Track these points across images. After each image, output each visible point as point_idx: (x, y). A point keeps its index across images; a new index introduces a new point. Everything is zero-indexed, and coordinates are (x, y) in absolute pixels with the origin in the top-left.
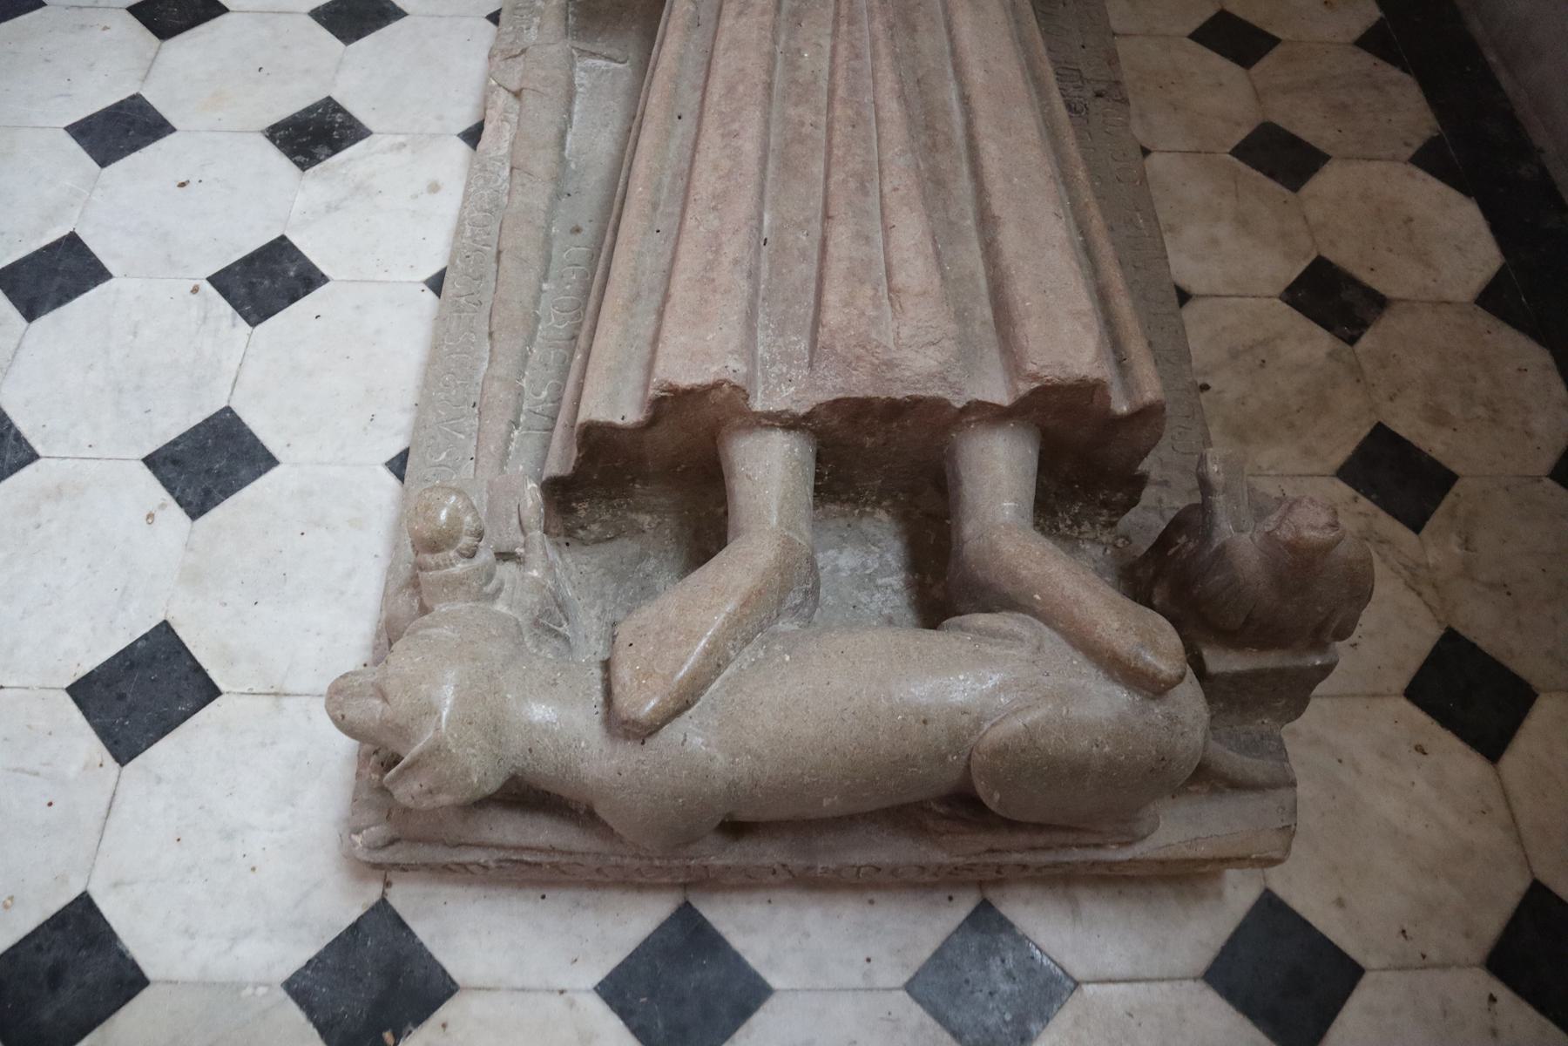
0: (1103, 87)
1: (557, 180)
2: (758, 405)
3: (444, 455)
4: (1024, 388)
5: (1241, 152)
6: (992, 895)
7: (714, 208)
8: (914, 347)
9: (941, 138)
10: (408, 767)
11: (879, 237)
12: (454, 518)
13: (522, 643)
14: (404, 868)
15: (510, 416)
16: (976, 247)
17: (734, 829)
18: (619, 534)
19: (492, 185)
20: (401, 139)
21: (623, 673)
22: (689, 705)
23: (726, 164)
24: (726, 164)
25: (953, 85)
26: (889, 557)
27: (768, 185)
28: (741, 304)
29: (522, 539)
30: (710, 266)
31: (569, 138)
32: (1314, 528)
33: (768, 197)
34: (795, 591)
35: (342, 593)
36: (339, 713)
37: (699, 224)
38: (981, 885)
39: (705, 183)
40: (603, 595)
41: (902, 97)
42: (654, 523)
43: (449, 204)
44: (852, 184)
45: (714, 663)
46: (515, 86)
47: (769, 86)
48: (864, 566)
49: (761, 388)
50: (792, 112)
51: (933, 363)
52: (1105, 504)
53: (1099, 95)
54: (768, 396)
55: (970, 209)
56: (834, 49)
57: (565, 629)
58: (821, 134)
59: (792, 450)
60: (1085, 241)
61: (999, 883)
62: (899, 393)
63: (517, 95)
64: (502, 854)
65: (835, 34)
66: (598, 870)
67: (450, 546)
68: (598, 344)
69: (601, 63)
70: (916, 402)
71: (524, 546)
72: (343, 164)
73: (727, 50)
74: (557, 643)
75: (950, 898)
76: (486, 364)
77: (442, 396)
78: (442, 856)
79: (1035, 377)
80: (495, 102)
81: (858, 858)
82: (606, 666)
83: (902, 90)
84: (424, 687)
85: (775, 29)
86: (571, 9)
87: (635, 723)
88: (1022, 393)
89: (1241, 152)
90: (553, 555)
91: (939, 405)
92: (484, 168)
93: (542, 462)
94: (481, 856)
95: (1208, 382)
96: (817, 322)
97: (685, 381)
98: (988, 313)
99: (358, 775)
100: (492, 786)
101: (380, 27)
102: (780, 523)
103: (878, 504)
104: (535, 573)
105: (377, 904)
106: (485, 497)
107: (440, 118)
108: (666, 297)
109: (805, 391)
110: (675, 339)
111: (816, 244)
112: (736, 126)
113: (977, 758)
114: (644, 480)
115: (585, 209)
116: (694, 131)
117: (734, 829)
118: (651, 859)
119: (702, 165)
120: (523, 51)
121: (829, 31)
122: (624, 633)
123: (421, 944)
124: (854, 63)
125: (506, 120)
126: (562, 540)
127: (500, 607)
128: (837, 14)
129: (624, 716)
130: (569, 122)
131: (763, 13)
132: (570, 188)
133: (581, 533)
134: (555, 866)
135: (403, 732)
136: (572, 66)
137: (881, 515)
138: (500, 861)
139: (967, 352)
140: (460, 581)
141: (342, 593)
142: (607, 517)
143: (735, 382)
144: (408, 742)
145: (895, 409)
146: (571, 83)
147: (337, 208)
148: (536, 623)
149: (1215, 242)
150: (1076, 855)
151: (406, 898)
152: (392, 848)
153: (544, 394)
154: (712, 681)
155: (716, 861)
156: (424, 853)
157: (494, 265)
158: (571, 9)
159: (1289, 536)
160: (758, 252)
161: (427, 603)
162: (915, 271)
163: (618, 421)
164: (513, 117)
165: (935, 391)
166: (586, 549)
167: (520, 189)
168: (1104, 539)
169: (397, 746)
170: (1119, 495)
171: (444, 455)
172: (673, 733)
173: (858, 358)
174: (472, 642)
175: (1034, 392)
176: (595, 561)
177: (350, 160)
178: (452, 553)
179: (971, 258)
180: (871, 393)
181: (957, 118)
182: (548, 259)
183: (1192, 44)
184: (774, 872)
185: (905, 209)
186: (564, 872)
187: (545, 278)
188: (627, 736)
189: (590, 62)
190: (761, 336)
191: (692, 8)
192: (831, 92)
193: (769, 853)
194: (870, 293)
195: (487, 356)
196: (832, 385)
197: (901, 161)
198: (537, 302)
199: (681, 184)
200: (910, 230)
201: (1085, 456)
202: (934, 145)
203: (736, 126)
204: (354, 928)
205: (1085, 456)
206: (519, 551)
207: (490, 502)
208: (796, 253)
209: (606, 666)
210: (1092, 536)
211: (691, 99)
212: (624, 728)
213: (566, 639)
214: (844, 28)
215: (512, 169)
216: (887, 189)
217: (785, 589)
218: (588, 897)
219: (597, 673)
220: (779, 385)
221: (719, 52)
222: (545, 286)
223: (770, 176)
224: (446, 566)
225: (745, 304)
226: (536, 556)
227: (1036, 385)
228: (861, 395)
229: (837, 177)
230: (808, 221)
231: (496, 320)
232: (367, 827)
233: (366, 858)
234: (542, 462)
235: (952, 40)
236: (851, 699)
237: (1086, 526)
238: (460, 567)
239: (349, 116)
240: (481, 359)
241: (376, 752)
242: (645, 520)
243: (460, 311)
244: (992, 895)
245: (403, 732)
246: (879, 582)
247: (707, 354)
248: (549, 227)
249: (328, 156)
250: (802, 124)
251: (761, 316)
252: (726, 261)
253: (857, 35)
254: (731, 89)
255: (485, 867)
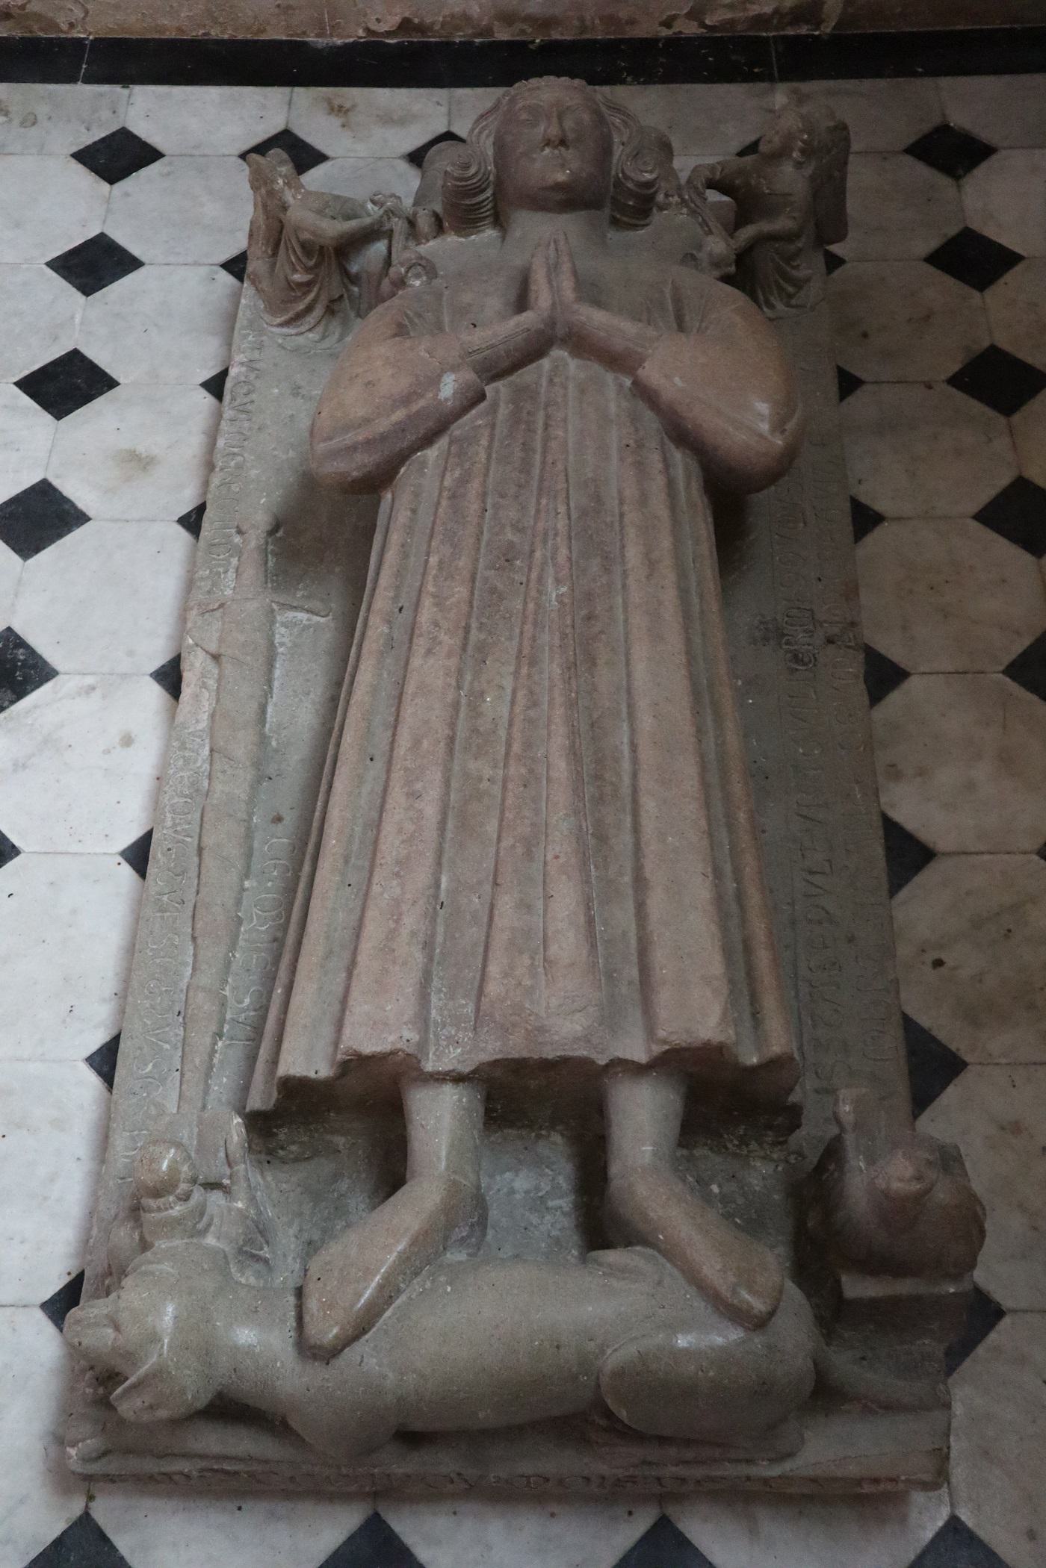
0: (836, 630)
1: (257, 764)
2: (429, 1066)
3: (150, 1066)
4: (657, 1049)
5: (1017, 670)
6: (671, 1511)
7: (397, 875)
8: (563, 1019)
9: (608, 789)
10: (134, 1386)
11: (540, 904)
12: (173, 1169)
13: (230, 1273)
14: (110, 1479)
15: (214, 1028)
16: (630, 905)
17: (411, 1438)
18: (316, 1154)
19: (191, 766)
20: (90, 680)
21: (312, 1304)
22: (364, 1331)
23: (410, 827)
24: (410, 827)
25: (625, 726)
26: (561, 1180)
27: (447, 846)
28: (415, 976)
29: (228, 1171)
30: (392, 935)
31: (270, 709)
32: (901, 1180)
33: (445, 860)
34: (467, 1219)
35: (45, 1198)
36: (76, 1341)
37: (385, 889)
38: (662, 1499)
39: (391, 846)
40: (301, 1214)
41: (574, 754)
42: (347, 1141)
43: (144, 760)
44: (520, 850)
45: (387, 1295)
46: (213, 647)
47: (451, 740)
48: (537, 1189)
49: (432, 1049)
50: (473, 766)
51: (578, 1028)
52: (770, 1127)
53: (830, 641)
54: (439, 1058)
55: (628, 866)
56: (514, 692)
57: (266, 1253)
58: (496, 790)
59: (460, 1100)
60: (738, 889)
61: (679, 1498)
62: (550, 1053)
63: (216, 658)
64: (204, 1464)
65: (516, 674)
66: (292, 1479)
67: (170, 1193)
68: (296, 1000)
69: (302, 616)
70: (565, 1061)
71: (231, 1177)
72: (28, 712)
73: (415, 695)
74: (259, 1266)
75: (630, 1513)
76: (189, 970)
77: (147, 1003)
78: (149, 1466)
79: (665, 1042)
80: (192, 665)
81: (526, 1467)
82: (299, 1293)
83: (572, 746)
84: (150, 1319)
85: (460, 672)
86: (270, 547)
87: (321, 1347)
88: (655, 1054)
89: (1017, 670)
90: (256, 1178)
91: (585, 1063)
92: (183, 747)
93: (246, 1088)
94: (185, 1466)
95: (943, 956)
96: (481, 992)
97: (368, 1048)
98: (635, 973)
99: (72, 1389)
100: (202, 1403)
101: (60, 536)
102: (448, 1168)
103: (552, 1127)
104: (240, 1205)
105: (80, 1518)
106: (196, 1130)
107: (131, 653)
108: (353, 964)
109: (470, 1052)
110: (360, 1007)
111: (487, 906)
112: (418, 786)
113: (605, 1380)
114: (335, 1122)
115: (286, 794)
116: (384, 777)
117: (411, 1438)
118: (339, 1467)
119: (388, 828)
120: (221, 606)
121: (512, 669)
122: (314, 1267)
123: (122, 1558)
124: (532, 713)
125: (204, 686)
126: (263, 1157)
127: (210, 1240)
128: (520, 651)
129: (312, 1341)
130: (268, 693)
131: (449, 656)
132: (271, 769)
133: (281, 1153)
134: (252, 1475)
135: (131, 1357)
136: (273, 622)
137: (557, 1138)
138: (202, 1470)
139: (610, 1017)
140: (178, 1221)
141: (45, 1198)
142: (305, 1139)
143: (410, 1051)
144: (134, 1364)
145: (547, 1066)
146: (271, 646)
147: (24, 766)
148: (240, 1251)
149: (970, 786)
150: (731, 1470)
151: (106, 1512)
152: (104, 1460)
153: (247, 1001)
154: (384, 1311)
155: (398, 1469)
156: (134, 1464)
157: (196, 859)
158: (270, 547)
159: (884, 1186)
160: (433, 920)
161: (148, 1238)
162: (567, 945)
163: (312, 1075)
164: (212, 683)
165: (581, 1052)
166: (286, 1167)
167: (219, 774)
168: (775, 1156)
169: (121, 1365)
170: (780, 1119)
171: (150, 1066)
172: (351, 1354)
173: (514, 1025)
174: (189, 1278)
175: (666, 1052)
176: (294, 1179)
177: (36, 707)
178: (171, 1198)
179: (624, 916)
180: (525, 1054)
181: (626, 766)
182: (249, 854)
183: (975, 525)
184: (452, 1482)
185: (564, 877)
186: (259, 1481)
187: (247, 875)
188: (315, 1357)
189: (291, 614)
190: (434, 999)
191: (387, 631)
192: (509, 745)
193: (445, 1463)
194: (527, 961)
195: (190, 960)
196: (491, 1049)
197: (565, 826)
198: (238, 903)
199: (371, 835)
200: (566, 899)
201: (721, 1100)
202: (601, 797)
203: (418, 786)
204: (58, 1543)
205: (721, 1100)
206: (226, 1181)
207: (199, 1135)
208: (468, 917)
209: (299, 1293)
210: (762, 1154)
211: (382, 737)
212: (309, 1350)
213: (266, 1261)
214: (524, 671)
215: (211, 750)
216: (549, 857)
217: (450, 1226)
218: (282, 1507)
219: (292, 1300)
220: (448, 1046)
221: (407, 698)
222: (247, 884)
223: (449, 835)
224: (166, 1209)
225: (420, 974)
226: (241, 1189)
227: (667, 1047)
228: (517, 1056)
229: (504, 844)
230: (480, 883)
231: (199, 925)
232: (83, 1440)
233: (79, 1470)
234: (246, 1088)
235: (629, 675)
236: (497, 1326)
237: (754, 1145)
238: (178, 1210)
239: (32, 652)
240: (185, 964)
241: (92, 1368)
242: (340, 1141)
243: (162, 910)
244: (671, 1511)
245: (131, 1357)
246: (550, 1204)
247: (386, 1024)
248: (250, 815)
249: (12, 702)
250: (480, 779)
251: (436, 979)
252: (405, 932)
253: (536, 678)
254: (417, 743)
255: (188, 1477)
